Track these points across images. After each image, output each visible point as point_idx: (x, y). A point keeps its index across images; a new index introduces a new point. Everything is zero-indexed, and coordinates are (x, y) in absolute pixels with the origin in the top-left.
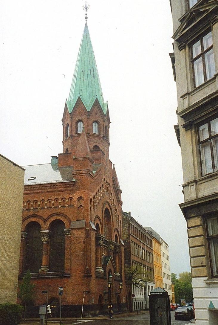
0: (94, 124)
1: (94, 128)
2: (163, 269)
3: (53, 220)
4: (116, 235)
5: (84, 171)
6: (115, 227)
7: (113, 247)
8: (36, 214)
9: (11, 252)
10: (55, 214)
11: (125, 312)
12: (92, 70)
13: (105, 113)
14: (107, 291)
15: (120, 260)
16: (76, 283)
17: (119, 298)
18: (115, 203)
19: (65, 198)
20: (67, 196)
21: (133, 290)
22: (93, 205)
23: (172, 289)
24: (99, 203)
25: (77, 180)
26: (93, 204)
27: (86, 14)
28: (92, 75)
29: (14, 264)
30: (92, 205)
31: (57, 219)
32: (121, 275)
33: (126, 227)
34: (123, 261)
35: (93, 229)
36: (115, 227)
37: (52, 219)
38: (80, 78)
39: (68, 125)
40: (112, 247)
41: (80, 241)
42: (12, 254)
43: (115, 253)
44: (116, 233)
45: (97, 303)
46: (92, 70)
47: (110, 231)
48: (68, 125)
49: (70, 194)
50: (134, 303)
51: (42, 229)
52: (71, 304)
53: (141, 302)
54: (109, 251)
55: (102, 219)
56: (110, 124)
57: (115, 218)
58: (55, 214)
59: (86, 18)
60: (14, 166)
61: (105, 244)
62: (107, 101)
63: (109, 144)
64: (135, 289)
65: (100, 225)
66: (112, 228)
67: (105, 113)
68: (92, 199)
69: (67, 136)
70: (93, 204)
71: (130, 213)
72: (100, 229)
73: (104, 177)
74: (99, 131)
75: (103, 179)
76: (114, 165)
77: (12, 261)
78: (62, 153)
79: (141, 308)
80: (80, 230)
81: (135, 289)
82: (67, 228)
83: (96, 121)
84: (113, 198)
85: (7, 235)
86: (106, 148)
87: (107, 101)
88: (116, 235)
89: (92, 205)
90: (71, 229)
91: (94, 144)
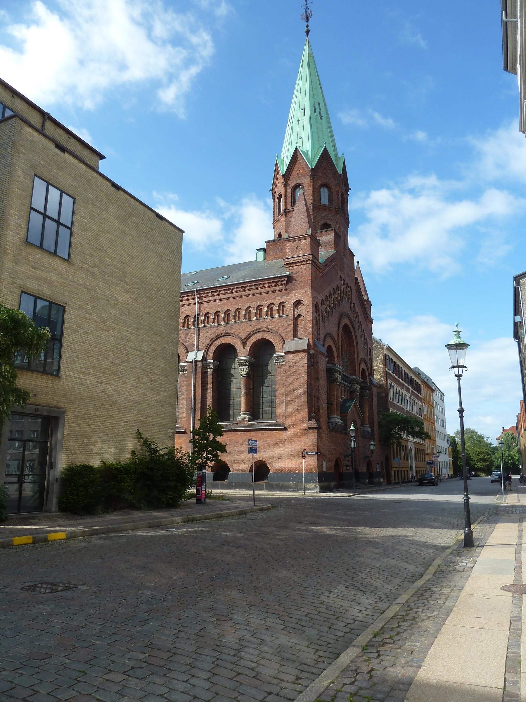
0: (322, 190)
1: (322, 196)
2: (437, 426)
3: (255, 340)
4: (363, 369)
5: (304, 257)
6: (360, 356)
7: (359, 387)
8: (229, 331)
9: (157, 375)
10: (260, 331)
11: (380, 484)
12: (317, 107)
13: (340, 171)
14: (349, 452)
15: (371, 407)
16: (295, 439)
17: (369, 465)
18: (360, 319)
19: (273, 304)
20: (277, 300)
21: (392, 454)
22: (321, 314)
23: (449, 454)
24: (332, 314)
25: (293, 273)
26: (320, 312)
27: (307, 26)
28: (318, 114)
29: (166, 396)
30: (319, 315)
31: (262, 337)
32: (373, 430)
33: (379, 360)
34: (375, 409)
35: (323, 354)
36: (360, 356)
37: (254, 339)
38: (299, 121)
39: (280, 196)
40: (357, 387)
41: (300, 371)
42: (159, 378)
43: (362, 397)
44: (363, 366)
45: (332, 470)
46: (317, 107)
47: (353, 361)
48: (280, 196)
49: (282, 296)
50: (395, 471)
51: (239, 354)
52: (288, 471)
53: (404, 471)
54: (351, 393)
55: (338, 336)
56: (350, 192)
57: (360, 343)
58: (260, 331)
59: (308, 32)
60: (158, 220)
61: (344, 381)
62: (343, 155)
63: (348, 223)
64: (395, 449)
65: (334, 349)
66: (356, 358)
67: (340, 171)
68: (320, 305)
69: (279, 212)
70: (320, 312)
71: (350, 189)
72: (335, 355)
73: (340, 273)
74: (330, 200)
75: (338, 277)
76: (358, 262)
77: (161, 391)
78: (273, 238)
79: (405, 479)
80: (300, 354)
81: (395, 449)
82: (278, 352)
83: (324, 185)
84: (357, 310)
85: (148, 343)
86: (343, 229)
87: (343, 155)
88: (363, 369)
89: (319, 315)
90: (285, 353)
91: (323, 222)
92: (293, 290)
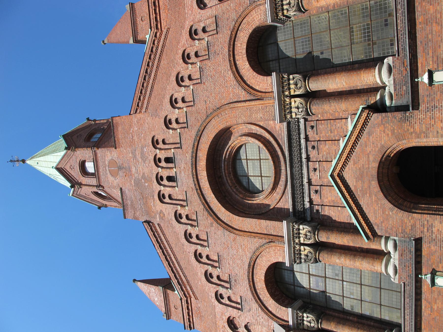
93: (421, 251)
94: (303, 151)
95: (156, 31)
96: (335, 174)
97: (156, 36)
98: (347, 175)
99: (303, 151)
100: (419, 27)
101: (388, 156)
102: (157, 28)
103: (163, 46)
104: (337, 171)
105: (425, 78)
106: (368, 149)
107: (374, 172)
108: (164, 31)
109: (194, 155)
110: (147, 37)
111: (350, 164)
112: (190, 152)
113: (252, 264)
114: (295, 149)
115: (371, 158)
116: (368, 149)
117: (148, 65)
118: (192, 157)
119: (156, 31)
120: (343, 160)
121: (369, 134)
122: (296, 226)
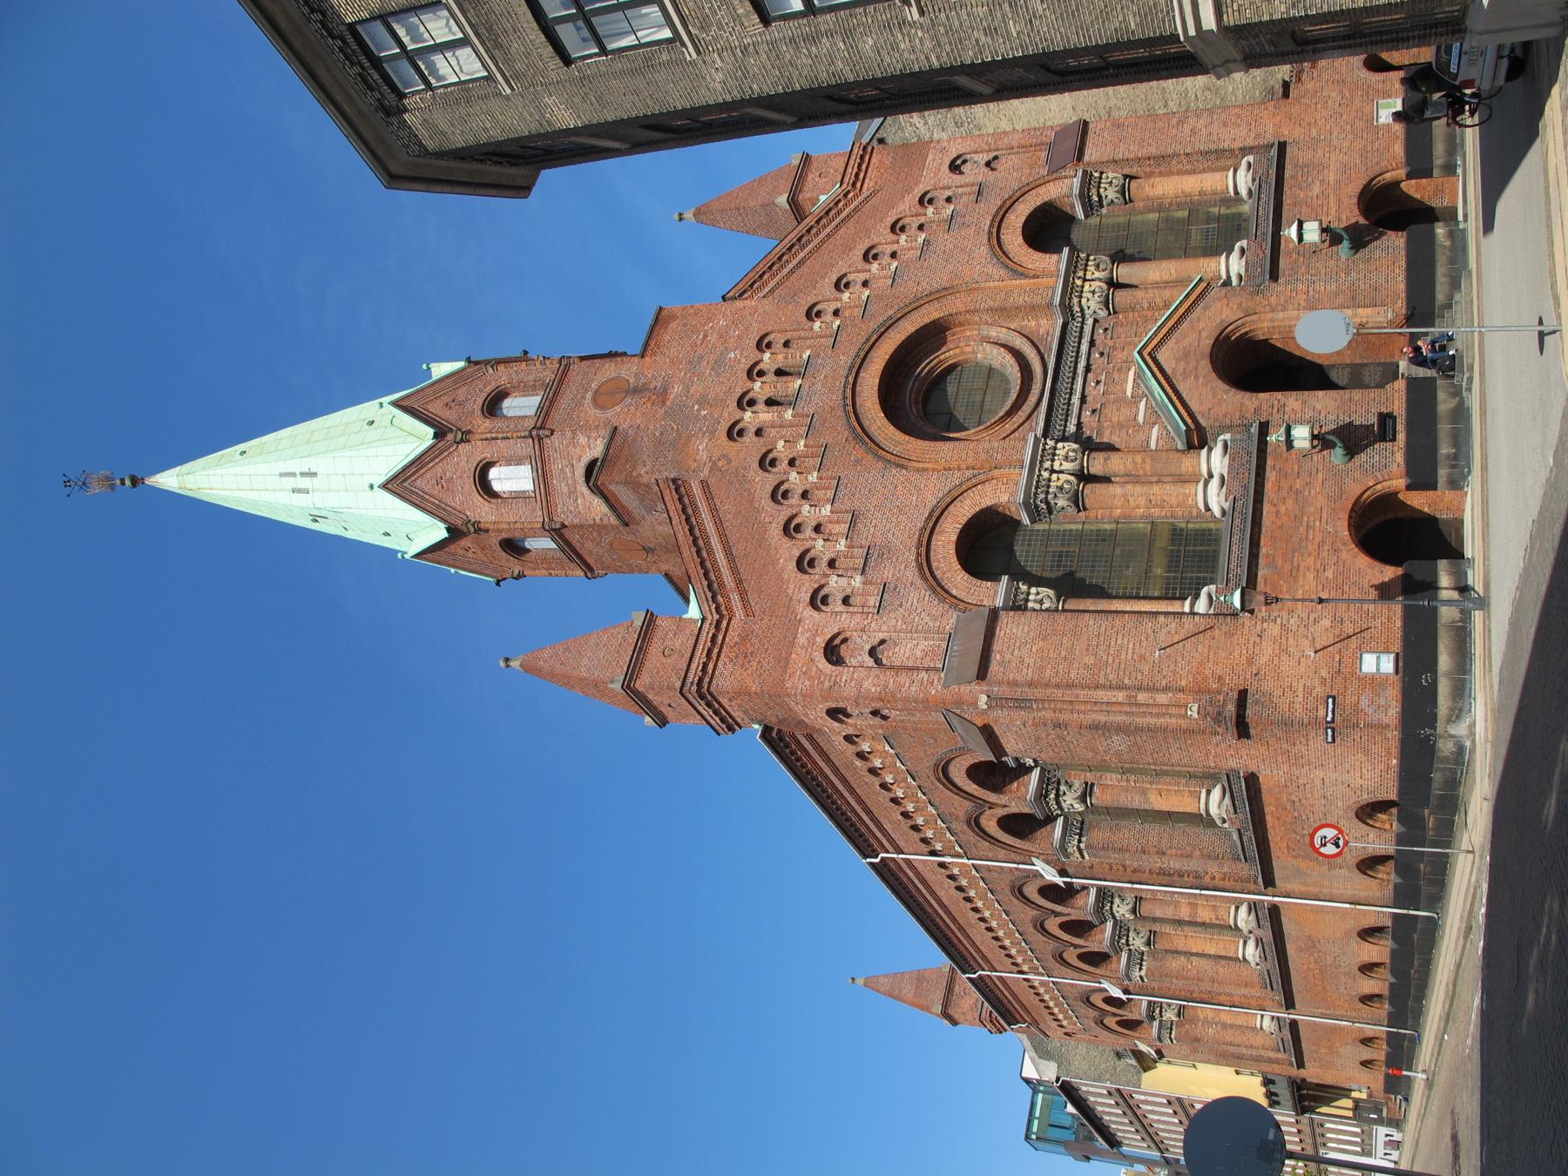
92: (801, 722)
93: (1263, 486)
94: (1080, 380)
95: (716, 617)
96: (1145, 354)
97: (846, 195)
98: (1164, 356)
99: (1080, 380)
100: (1285, 208)
101: (1228, 337)
102: (854, 184)
103: (856, 210)
104: (1149, 349)
105: (1293, 232)
106: (1201, 326)
107: (1207, 351)
108: (865, 193)
109: (862, 354)
110: (823, 198)
111: (1171, 343)
112: (852, 353)
113: (937, 513)
114: (1069, 358)
115: (1204, 334)
116: (1201, 326)
117: (808, 231)
118: (857, 355)
119: (716, 617)
120: (1161, 335)
121: (1206, 308)
122: (1024, 588)
